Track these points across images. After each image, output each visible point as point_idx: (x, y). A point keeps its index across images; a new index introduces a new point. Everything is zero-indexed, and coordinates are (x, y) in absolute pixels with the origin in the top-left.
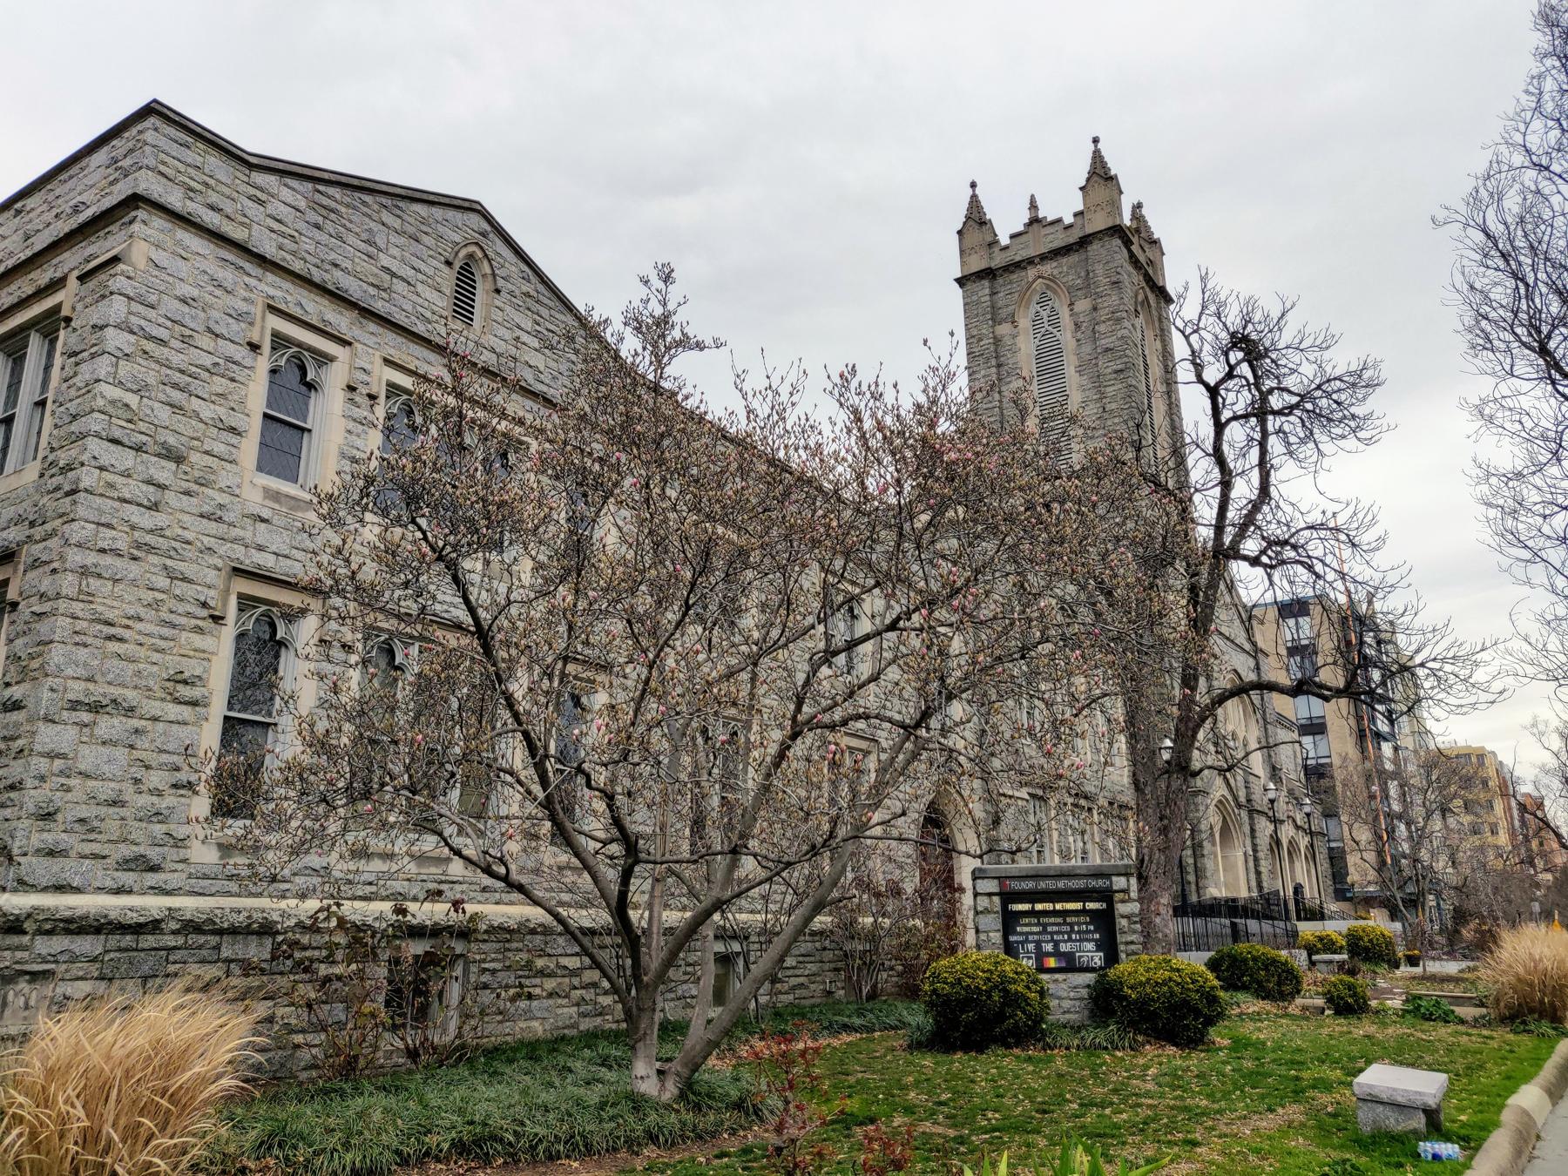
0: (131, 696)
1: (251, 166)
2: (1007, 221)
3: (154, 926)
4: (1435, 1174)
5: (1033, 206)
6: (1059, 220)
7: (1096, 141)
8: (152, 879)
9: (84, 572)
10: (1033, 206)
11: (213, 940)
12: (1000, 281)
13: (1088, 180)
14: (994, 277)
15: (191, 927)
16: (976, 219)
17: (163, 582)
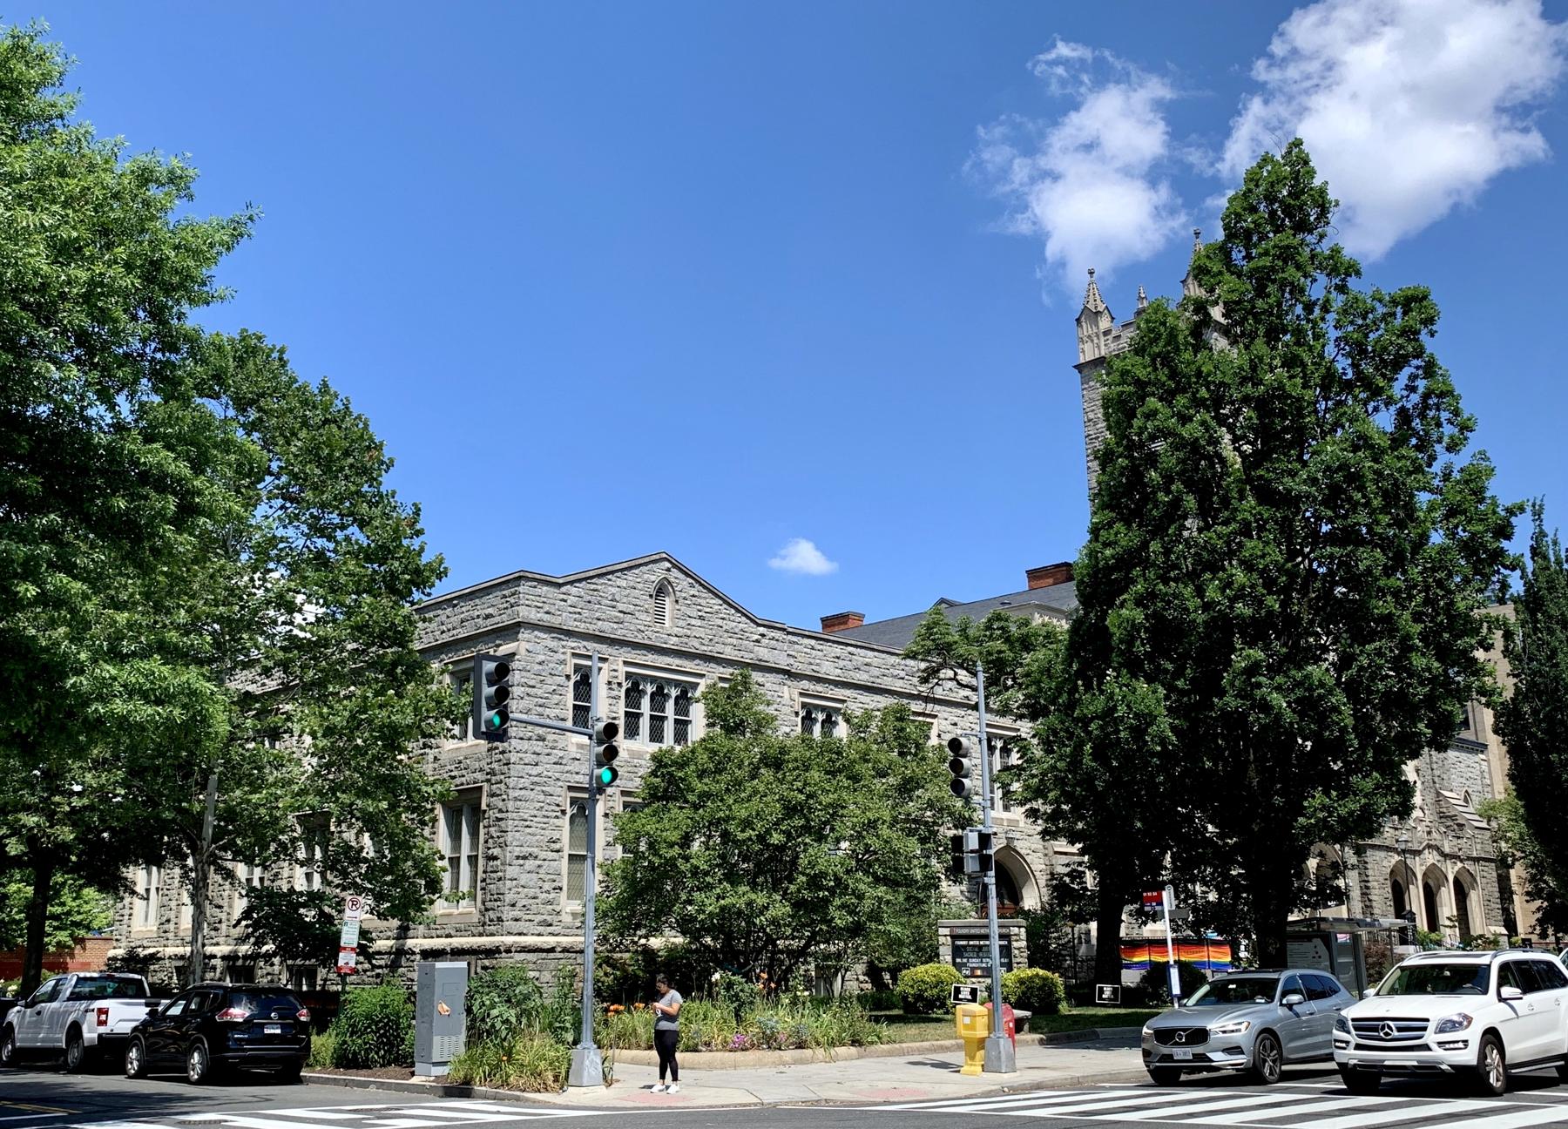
0: (535, 851)
1: (560, 585)
3: (552, 950)
8: (550, 929)
9: (516, 799)
15: (565, 950)
17: (542, 797)
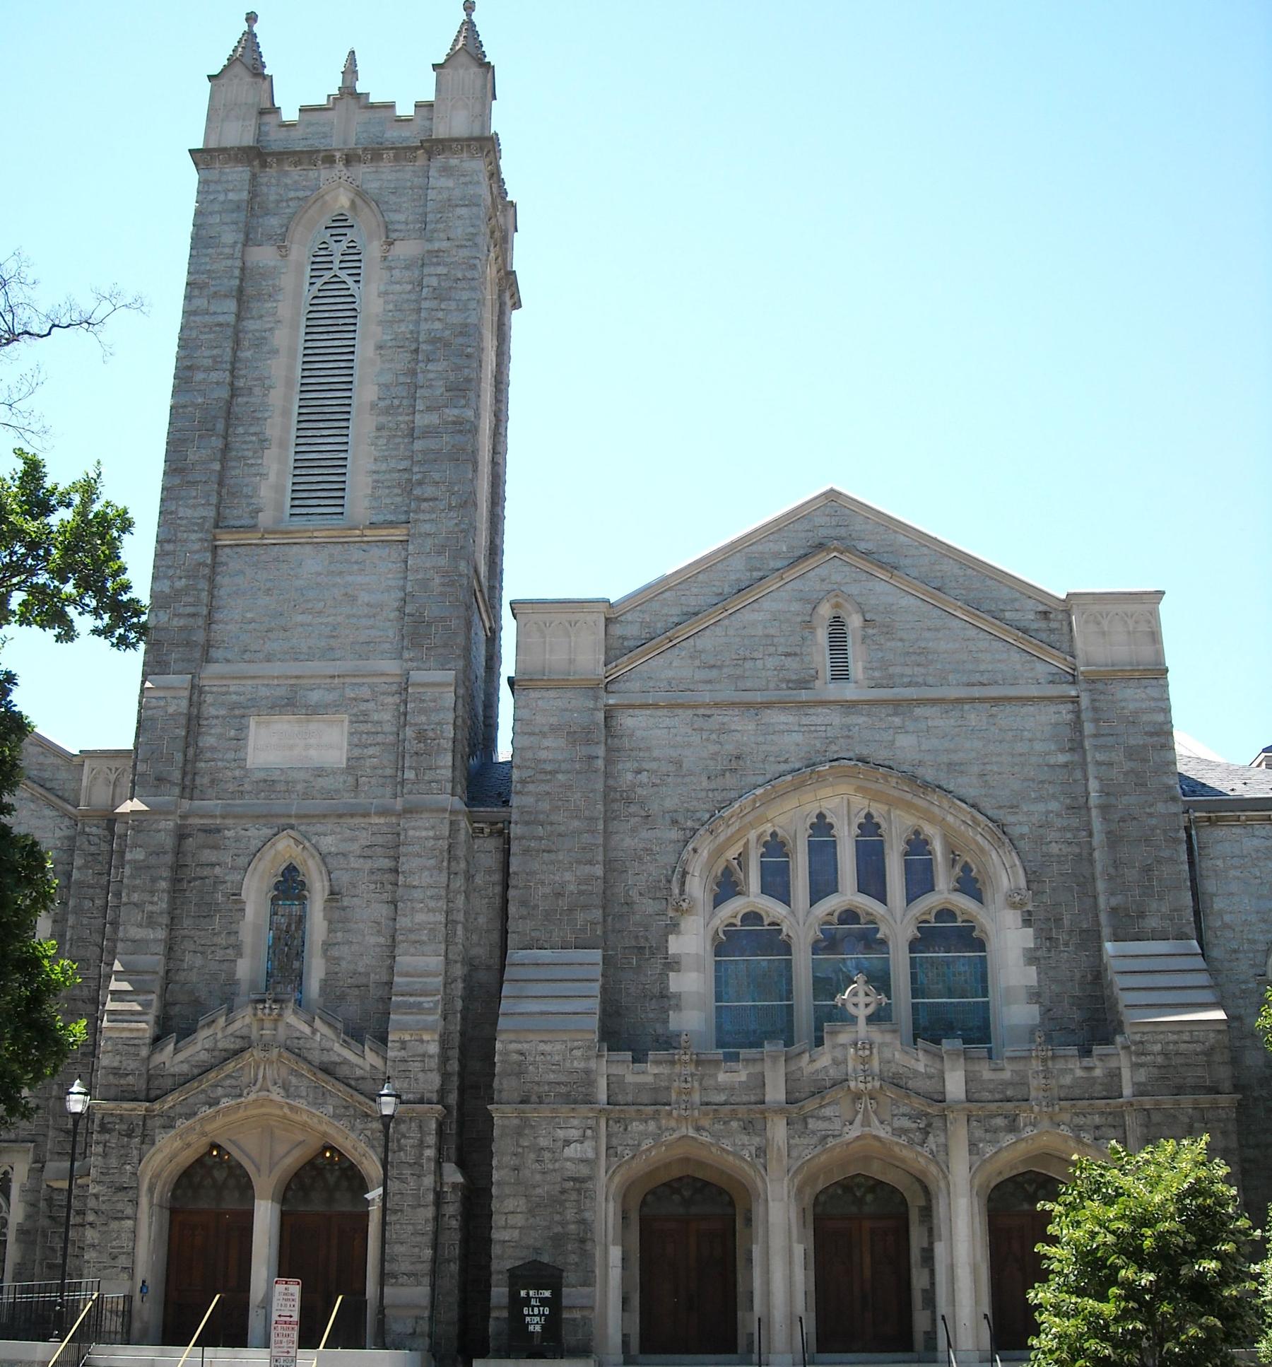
2: (299, 86)
4: (1, 1281)
5: (351, 70)
6: (390, 106)
7: (251, 18)
10: (351, 70)
11: (823, 728)
12: (272, 171)
13: (450, 57)
14: (264, 165)
16: (247, 61)
